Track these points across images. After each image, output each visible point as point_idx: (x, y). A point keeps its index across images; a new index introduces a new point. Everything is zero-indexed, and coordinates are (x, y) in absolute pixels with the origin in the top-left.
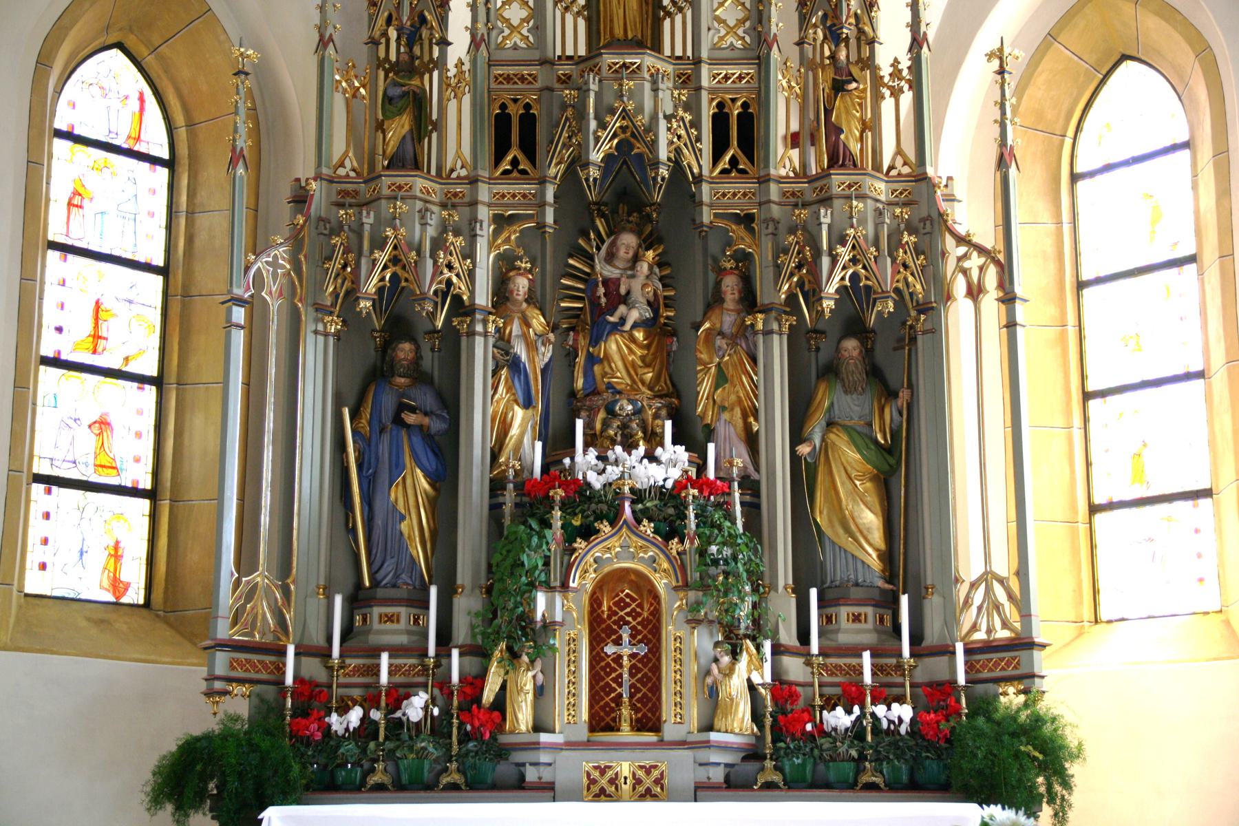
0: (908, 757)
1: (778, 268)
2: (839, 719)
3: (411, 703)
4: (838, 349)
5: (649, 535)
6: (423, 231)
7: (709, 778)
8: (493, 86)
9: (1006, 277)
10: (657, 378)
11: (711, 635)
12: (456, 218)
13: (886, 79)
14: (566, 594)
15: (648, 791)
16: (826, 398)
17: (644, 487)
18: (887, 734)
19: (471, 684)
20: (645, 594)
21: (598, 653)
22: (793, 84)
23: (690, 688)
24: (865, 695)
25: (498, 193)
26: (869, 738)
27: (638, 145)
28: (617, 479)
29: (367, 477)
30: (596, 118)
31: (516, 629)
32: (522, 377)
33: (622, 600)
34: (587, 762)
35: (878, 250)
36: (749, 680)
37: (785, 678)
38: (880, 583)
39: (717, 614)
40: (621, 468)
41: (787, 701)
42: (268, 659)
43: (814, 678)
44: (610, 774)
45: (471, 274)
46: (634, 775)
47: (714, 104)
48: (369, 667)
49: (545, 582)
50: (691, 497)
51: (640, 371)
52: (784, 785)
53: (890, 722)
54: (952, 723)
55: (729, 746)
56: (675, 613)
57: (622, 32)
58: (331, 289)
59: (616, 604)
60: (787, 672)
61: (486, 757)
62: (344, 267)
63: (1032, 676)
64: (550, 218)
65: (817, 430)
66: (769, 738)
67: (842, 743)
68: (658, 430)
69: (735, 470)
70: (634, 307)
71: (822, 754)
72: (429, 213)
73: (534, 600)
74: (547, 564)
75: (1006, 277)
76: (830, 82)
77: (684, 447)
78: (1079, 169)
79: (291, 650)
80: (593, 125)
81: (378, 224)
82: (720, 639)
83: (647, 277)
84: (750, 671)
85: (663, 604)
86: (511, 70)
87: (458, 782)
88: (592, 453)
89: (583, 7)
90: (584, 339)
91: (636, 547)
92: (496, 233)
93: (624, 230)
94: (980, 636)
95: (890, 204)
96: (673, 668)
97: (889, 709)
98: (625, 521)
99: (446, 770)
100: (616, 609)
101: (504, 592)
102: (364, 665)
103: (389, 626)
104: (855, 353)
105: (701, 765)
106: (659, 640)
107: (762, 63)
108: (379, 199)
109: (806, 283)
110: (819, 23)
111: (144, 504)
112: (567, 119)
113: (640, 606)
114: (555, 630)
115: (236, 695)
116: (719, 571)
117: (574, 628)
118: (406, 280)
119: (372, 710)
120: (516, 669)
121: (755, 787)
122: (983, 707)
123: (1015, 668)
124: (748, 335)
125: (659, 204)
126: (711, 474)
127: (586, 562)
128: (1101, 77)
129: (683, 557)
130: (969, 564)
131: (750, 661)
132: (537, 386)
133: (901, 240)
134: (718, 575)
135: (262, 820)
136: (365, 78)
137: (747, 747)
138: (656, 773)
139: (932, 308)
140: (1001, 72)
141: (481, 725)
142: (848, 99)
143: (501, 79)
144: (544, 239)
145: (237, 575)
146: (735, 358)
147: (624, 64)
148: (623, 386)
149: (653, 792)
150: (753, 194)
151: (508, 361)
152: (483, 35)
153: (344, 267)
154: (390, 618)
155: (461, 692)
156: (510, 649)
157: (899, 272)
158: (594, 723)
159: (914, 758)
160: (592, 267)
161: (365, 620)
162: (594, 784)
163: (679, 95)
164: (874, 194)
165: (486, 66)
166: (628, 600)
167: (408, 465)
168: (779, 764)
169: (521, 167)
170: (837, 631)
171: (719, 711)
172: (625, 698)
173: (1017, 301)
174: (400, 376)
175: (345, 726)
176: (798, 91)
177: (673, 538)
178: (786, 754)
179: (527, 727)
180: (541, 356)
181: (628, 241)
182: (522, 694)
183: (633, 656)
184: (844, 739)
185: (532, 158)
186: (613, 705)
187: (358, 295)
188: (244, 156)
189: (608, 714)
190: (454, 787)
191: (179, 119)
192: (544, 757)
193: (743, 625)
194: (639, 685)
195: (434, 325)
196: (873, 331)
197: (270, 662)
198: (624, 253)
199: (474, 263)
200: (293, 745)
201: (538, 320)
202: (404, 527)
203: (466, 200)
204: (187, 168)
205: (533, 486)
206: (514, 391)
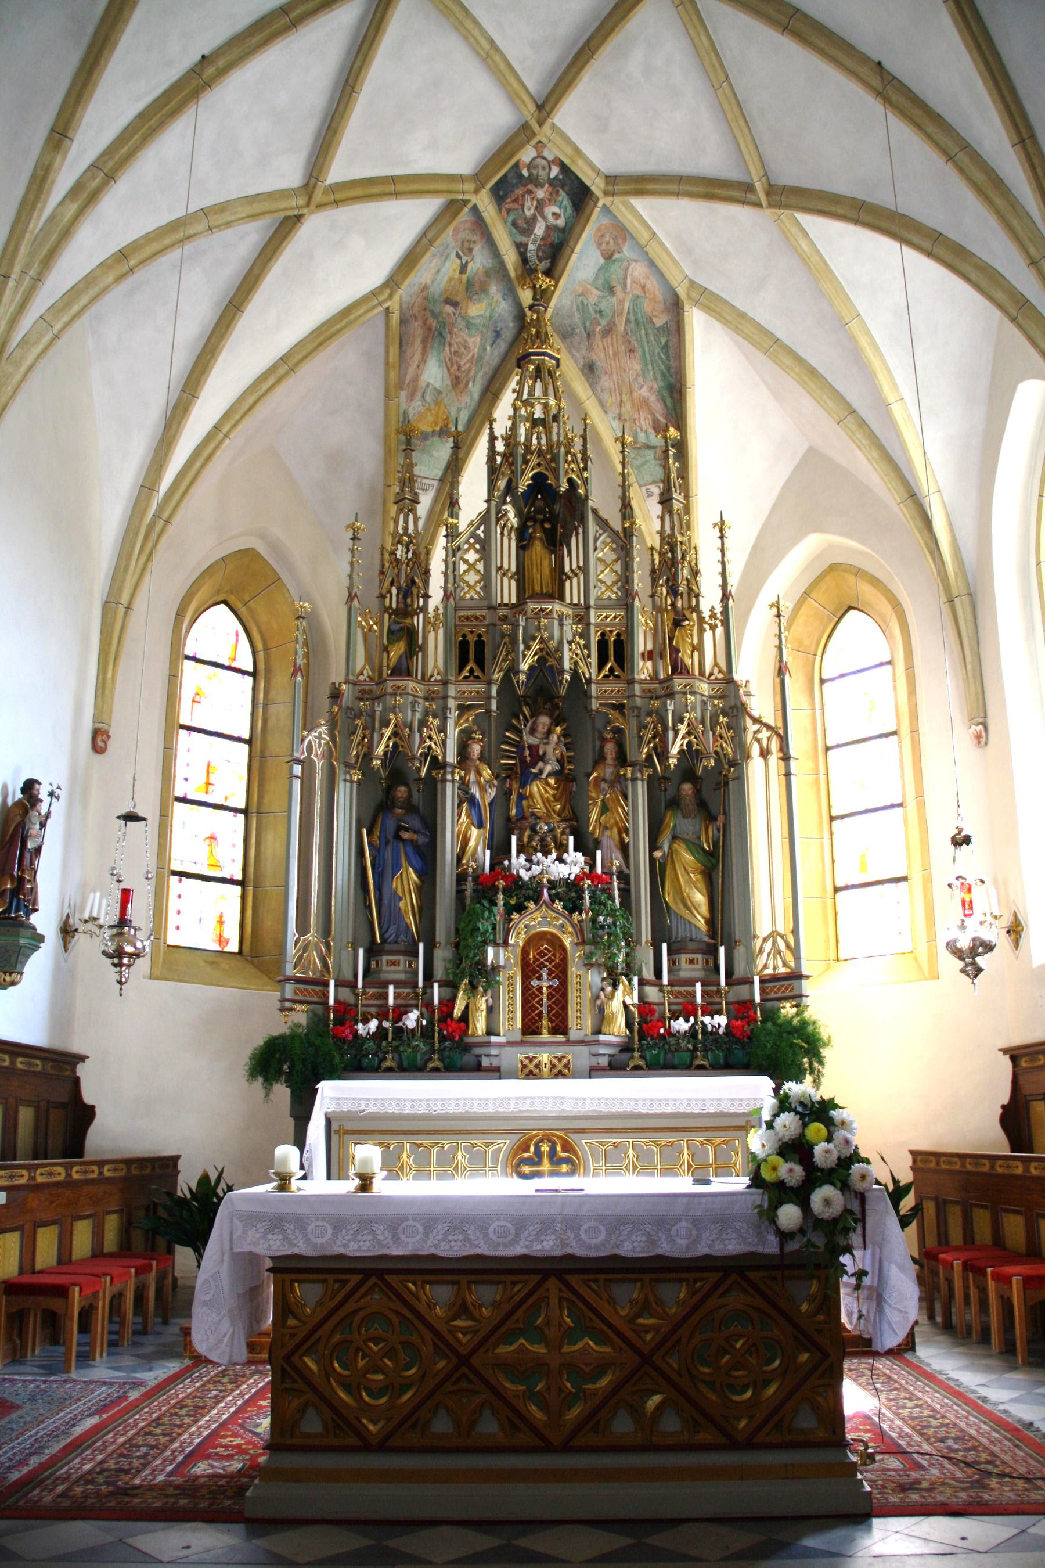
2: (681, 1025)
4: (679, 789)
6: (413, 715)
10: (563, 809)
11: (600, 973)
15: (560, 1072)
16: (671, 821)
18: (710, 1035)
23: (587, 1007)
26: (700, 1036)
34: (520, 1055)
36: (624, 1002)
37: (646, 1000)
38: (706, 939)
42: (318, 988)
44: (536, 1061)
45: (444, 742)
51: (553, 804)
53: (713, 1026)
54: (752, 1026)
59: (539, 954)
62: (363, 738)
63: (801, 996)
66: (636, 1038)
69: (614, 868)
73: (486, 952)
74: (494, 929)
79: (332, 983)
80: (522, 647)
83: (557, 744)
84: (624, 996)
86: (469, 613)
88: (523, 857)
92: (460, 716)
93: (540, 714)
94: (769, 971)
95: (711, 697)
99: (431, 1059)
103: (393, 968)
104: (690, 792)
106: (566, 977)
107: (629, 608)
108: (385, 695)
111: (238, 889)
113: (554, 955)
120: (475, 995)
122: (770, 1015)
130: (762, 926)
131: (625, 990)
138: (565, 1061)
140: (779, 616)
153: (363, 738)
154: (393, 963)
155: (440, 1010)
156: (470, 983)
160: (521, 737)
161: (377, 964)
164: (701, 691)
170: (679, 970)
172: (545, 1015)
181: (544, 720)
183: (549, 987)
185: (482, 667)
189: (533, 1024)
190: (436, 1070)
191: (260, 646)
192: (494, 1051)
196: (700, 778)
199: (445, 735)
202: (402, 904)
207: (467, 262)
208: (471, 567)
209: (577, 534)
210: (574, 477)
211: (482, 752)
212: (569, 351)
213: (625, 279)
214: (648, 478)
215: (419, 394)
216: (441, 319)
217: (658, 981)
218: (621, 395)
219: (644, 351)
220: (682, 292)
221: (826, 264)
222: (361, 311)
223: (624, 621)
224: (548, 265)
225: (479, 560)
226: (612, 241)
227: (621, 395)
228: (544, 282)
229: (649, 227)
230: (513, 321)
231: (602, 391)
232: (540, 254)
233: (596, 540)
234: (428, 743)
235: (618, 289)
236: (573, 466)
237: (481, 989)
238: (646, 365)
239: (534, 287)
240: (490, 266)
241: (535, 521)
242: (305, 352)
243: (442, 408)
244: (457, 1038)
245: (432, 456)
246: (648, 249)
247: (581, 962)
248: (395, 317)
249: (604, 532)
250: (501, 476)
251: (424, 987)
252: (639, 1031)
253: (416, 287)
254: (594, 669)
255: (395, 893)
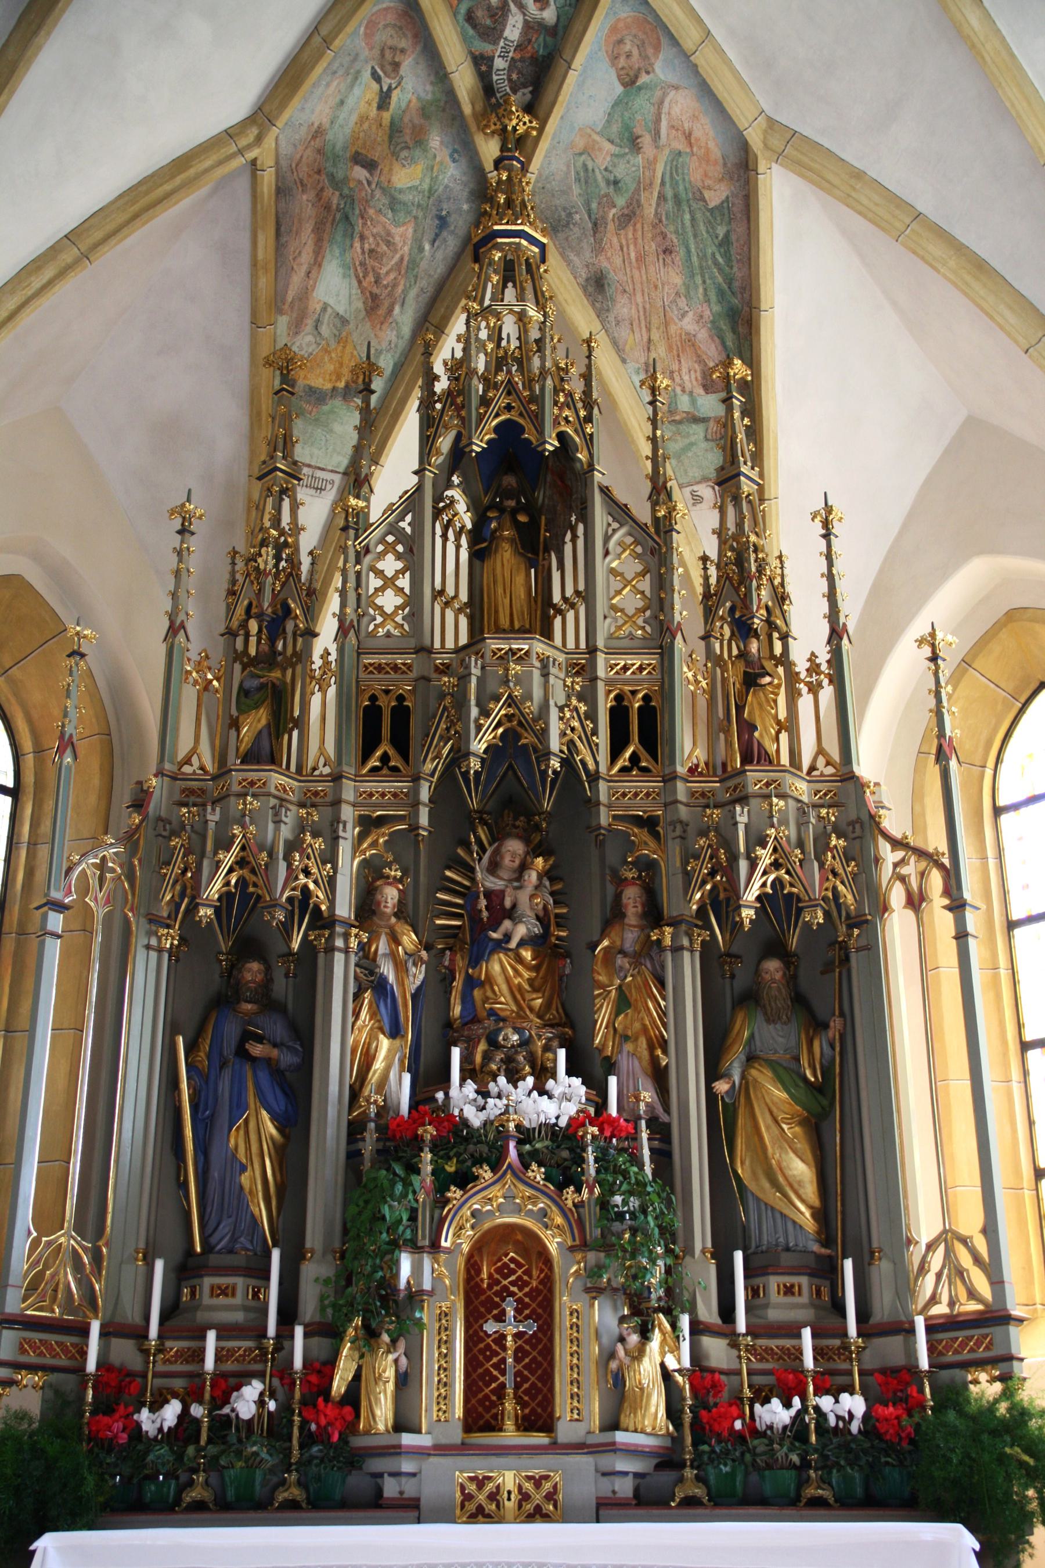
0: (863, 1462)
1: (687, 876)
3: (242, 1395)
4: (757, 972)
5: (538, 1183)
6: (277, 830)
7: (614, 1492)
8: (362, 675)
9: (953, 882)
10: (547, 1006)
11: (615, 1309)
12: (316, 818)
13: (803, 675)
14: (436, 1256)
15: (538, 1509)
17: (533, 1126)
19: (319, 1372)
20: (534, 1257)
21: (476, 1332)
22: (700, 678)
24: (806, 1384)
25: (364, 792)
26: (813, 1438)
27: (526, 735)
28: (501, 1114)
29: (204, 1120)
30: (478, 705)
31: (374, 1300)
32: (389, 1001)
33: (506, 1266)
35: (803, 852)
36: (663, 1365)
37: (705, 1364)
38: (815, 1247)
39: (623, 1280)
40: (505, 1101)
41: (709, 1392)
42: (69, 1340)
43: (741, 1363)
44: (490, 1487)
45: (332, 881)
46: (520, 1488)
47: (612, 696)
48: (194, 1351)
49: (411, 1240)
50: (589, 1137)
51: (528, 996)
52: (709, 1500)
53: (839, 1418)
54: (917, 1418)
55: (640, 1449)
56: (571, 1280)
57: (508, 623)
58: (168, 897)
59: (499, 1271)
60: (707, 1357)
61: (334, 1466)
62: (184, 872)
63: (1010, 1358)
64: (424, 819)
65: (736, 1064)
66: (689, 1440)
67: (780, 1444)
68: (549, 1065)
69: (642, 1106)
70: (521, 922)
71: (754, 1460)
72: (284, 810)
73: (397, 1263)
74: (413, 1218)
75: (953, 882)
76: (741, 676)
77: (580, 1079)
78: (1001, 802)
79: (95, 1327)
80: (474, 712)
81: (224, 824)
82: (626, 1313)
83: (537, 887)
84: (663, 1354)
85: (556, 1270)
86: (383, 659)
87: (298, 1498)
88: (470, 1087)
89: (465, 604)
90: (463, 959)
91: (522, 1197)
92: (362, 837)
93: (509, 835)
94: (941, 1309)
95: (815, 806)
96: (568, 1349)
97: (837, 1401)
98: (510, 1166)
99: (283, 1482)
100: (498, 1277)
101: (360, 1252)
102: (189, 1349)
103: (222, 1300)
104: (778, 976)
105: (604, 1474)
106: (551, 1315)
107: (666, 654)
108: (229, 795)
109: (721, 891)
110: (726, 615)
112: (445, 708)
113: (528, 1272)
114: (423, 1301)
115: (25, 1386)
116: (625, 1227)
117: (447, 1299)
118: (255, 885)
119: (194, 1405)
120: (373, 1351)
121: (673, 1504)
123: (987, 1348)
124: (653, 955)
125: (549, 813)
126: (613, 1110)
127: (462, 1217)
128: (1020, 705)
129: (581, 1210)
131: (663, 1342)
132: (407, 1014)
133: (829, 844)
134: (623, 1232)
135: (34, 1552)
136: (219, 670)
137: (661, 1451)
138: (547, 1486)
139: (867, 921)
140: (934, 658)
141: (329, 1424)
142: (761, 694)
143: (371, 669)
144: (417, 843)
145: (35, 1234)
146: (639, 979)
147: (510, 649)
148: (508, 1013)
149: (544, 1511)
150: (658, 795)
151: (372, 982)
152: (352, 621)
153: (184, 872)
154: (226, 1291)
156: (366, 1326)
157: (828, 879)
158: (470, 1420)
159: (871, 1466)
160: (473, 880)
161: (193, 1294)
162: (469, 1501)
163: (572, 683)
164: (795, 794)
165: (355, 654)
166: (512, 1266)
167: (252, 1105)
168: (702, 1473)
169: (392, 764)
170: (766, 1306)
171: (626, 1405)
172: (510, 1391)
173: (967, 908)
174: (247, 1001)
175: (158, 1425)
176: (705, 686)
177: (568, 1187)
178: (711, 1460)
179: (386, 1426)
180: (411, 978)
181: (514, 848)
182: (381, 1383)
183: (518, 1336)
184: (782, 1439)
185: (404, 752)
186: (494, 1398)
187: (198, 901)
188: (72, 743)
189: (487, 1410)
190: (292, 1505)
192: (407, 1466)
193: (653, 1296)
194: (526, 1373)
195: (289, 947)
196: (795, 955)
197: (72, 1345)
198: (509, 862)
199: (335, 868)
200: (91, 1451)
201: (410, 937)
202: (245, 1179)
203: (328, 799)
204: (32, 796)
205: (398, 1125)
206: (379, 1018)
207: (390, 89)
208: (389, 582)
209: (574, 540)
210: (569, 431)
211: (401, 902)
212: (563, 255)
213: (658, 121)
214: (696, 473)
215: (310, 322)
216: (346, 191)
217: (726, 1328)
218: (649, 330)
219: (689, 252)
220: (754, 137)
221: (1012, 56)
222: (208, 163)
223: (656, 675)
224: (529, 96)
225: (402, 572)
226: (635, 52)
227: (649, 330)
228: (519, 122)
229: (699, 21)
230: (468, 201)
231: (618, 323)
232: (514, 76)
233: (607, 539)
234: (302, 879)
235: (646, 141)
236: (566, 413)
237: (386, 1338)
238: (692, 276)
239: (504, 129)
240: (429, 97)
241: (502, 510)
242: (110, 227)
243: (349, 349)
244: (336, 1437)
245: (331, 431)
246: (698, 59)
247: (580, 1284)
248: (268, 178)
249: (622, 525)
250: (442, 430)
251: (278, 1336)
252: (692, 1425)
253: (304, 130)
254: (604, 756)
255: (234, 1156)
